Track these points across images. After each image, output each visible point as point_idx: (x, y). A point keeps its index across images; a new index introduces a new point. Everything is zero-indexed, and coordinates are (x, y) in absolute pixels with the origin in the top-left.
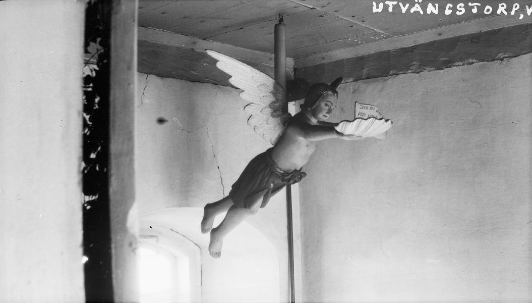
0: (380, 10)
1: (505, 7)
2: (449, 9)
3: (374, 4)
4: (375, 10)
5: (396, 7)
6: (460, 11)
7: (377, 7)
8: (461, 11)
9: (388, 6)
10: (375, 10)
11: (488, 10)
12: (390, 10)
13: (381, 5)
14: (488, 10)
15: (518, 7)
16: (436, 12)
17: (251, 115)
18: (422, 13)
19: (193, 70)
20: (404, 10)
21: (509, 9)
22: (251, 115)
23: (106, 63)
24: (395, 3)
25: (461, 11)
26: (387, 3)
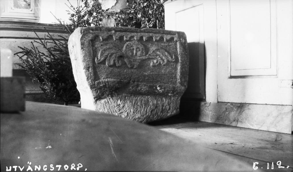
0: (10, 170)
1: (74, 166)
2: (256, 166)
3: (7, 167)
4: (7, 170)
5: (18, 168)
6: (52, 168)
7: (9, 169)
8: (45, 169)
9: (14, 169)
10: (7, 170)
11: (66, 167)
12: (15, 170)
13: (10, 167)
14: (66, 167)
15: (280, 162)
16: (39, 169)
17: (231, 77)
18: (32, 170)
19: (58, 54)
20: (21, 170)
21: (76, 167)
22: (231, 77)
23: (34, 67)
24: (17, 167)
25: (45, 169)
26: (14, 167)
